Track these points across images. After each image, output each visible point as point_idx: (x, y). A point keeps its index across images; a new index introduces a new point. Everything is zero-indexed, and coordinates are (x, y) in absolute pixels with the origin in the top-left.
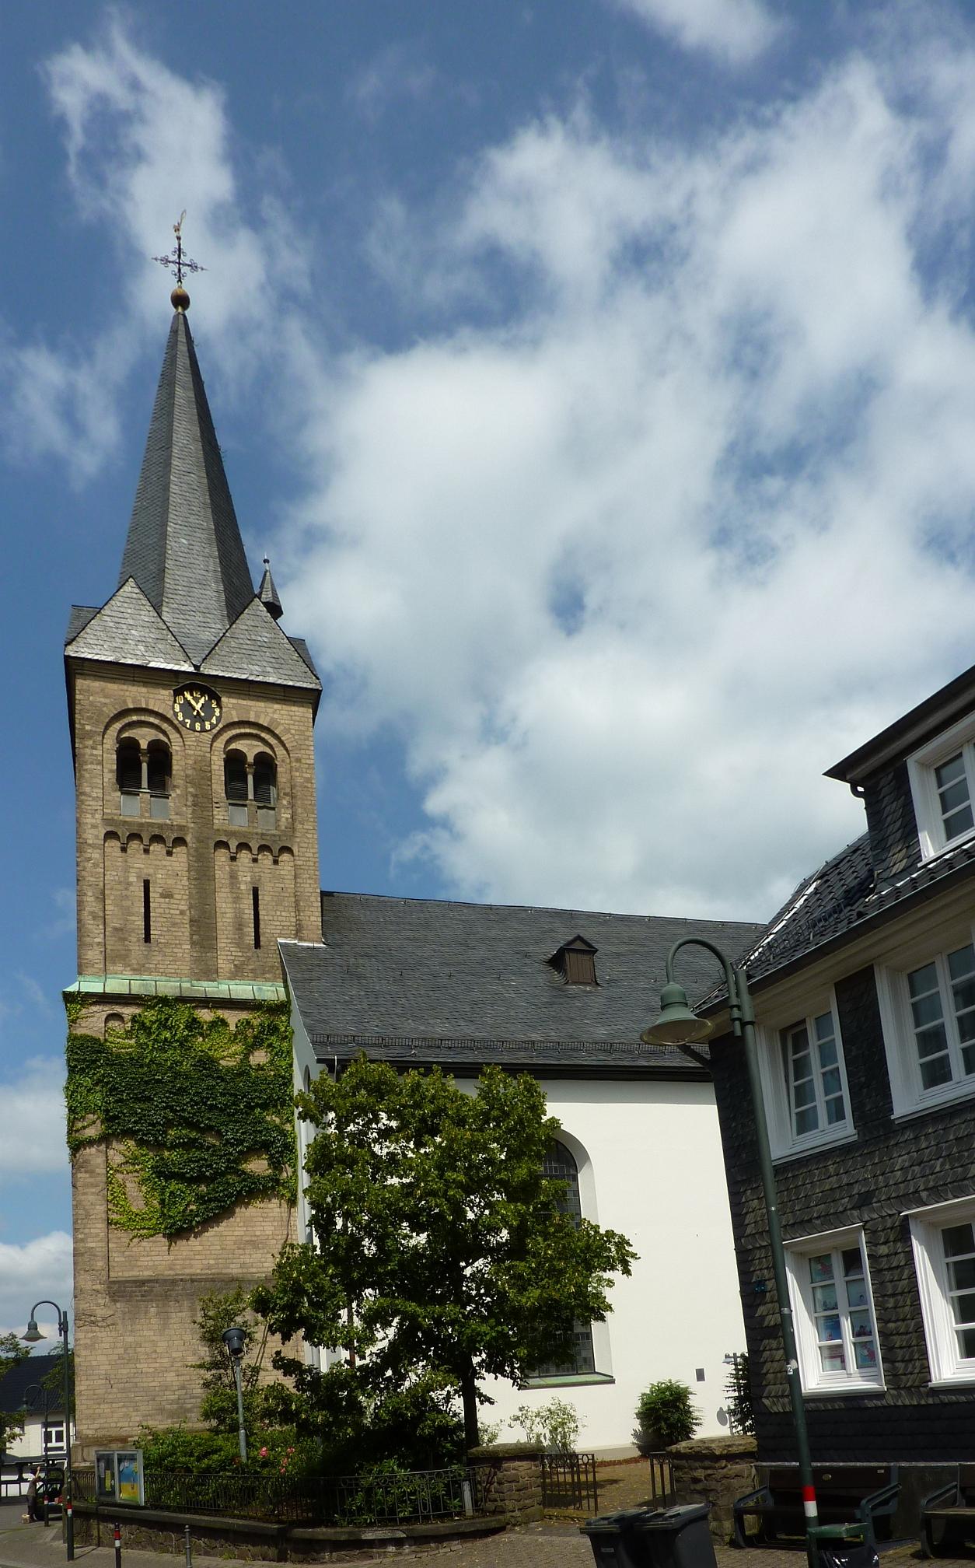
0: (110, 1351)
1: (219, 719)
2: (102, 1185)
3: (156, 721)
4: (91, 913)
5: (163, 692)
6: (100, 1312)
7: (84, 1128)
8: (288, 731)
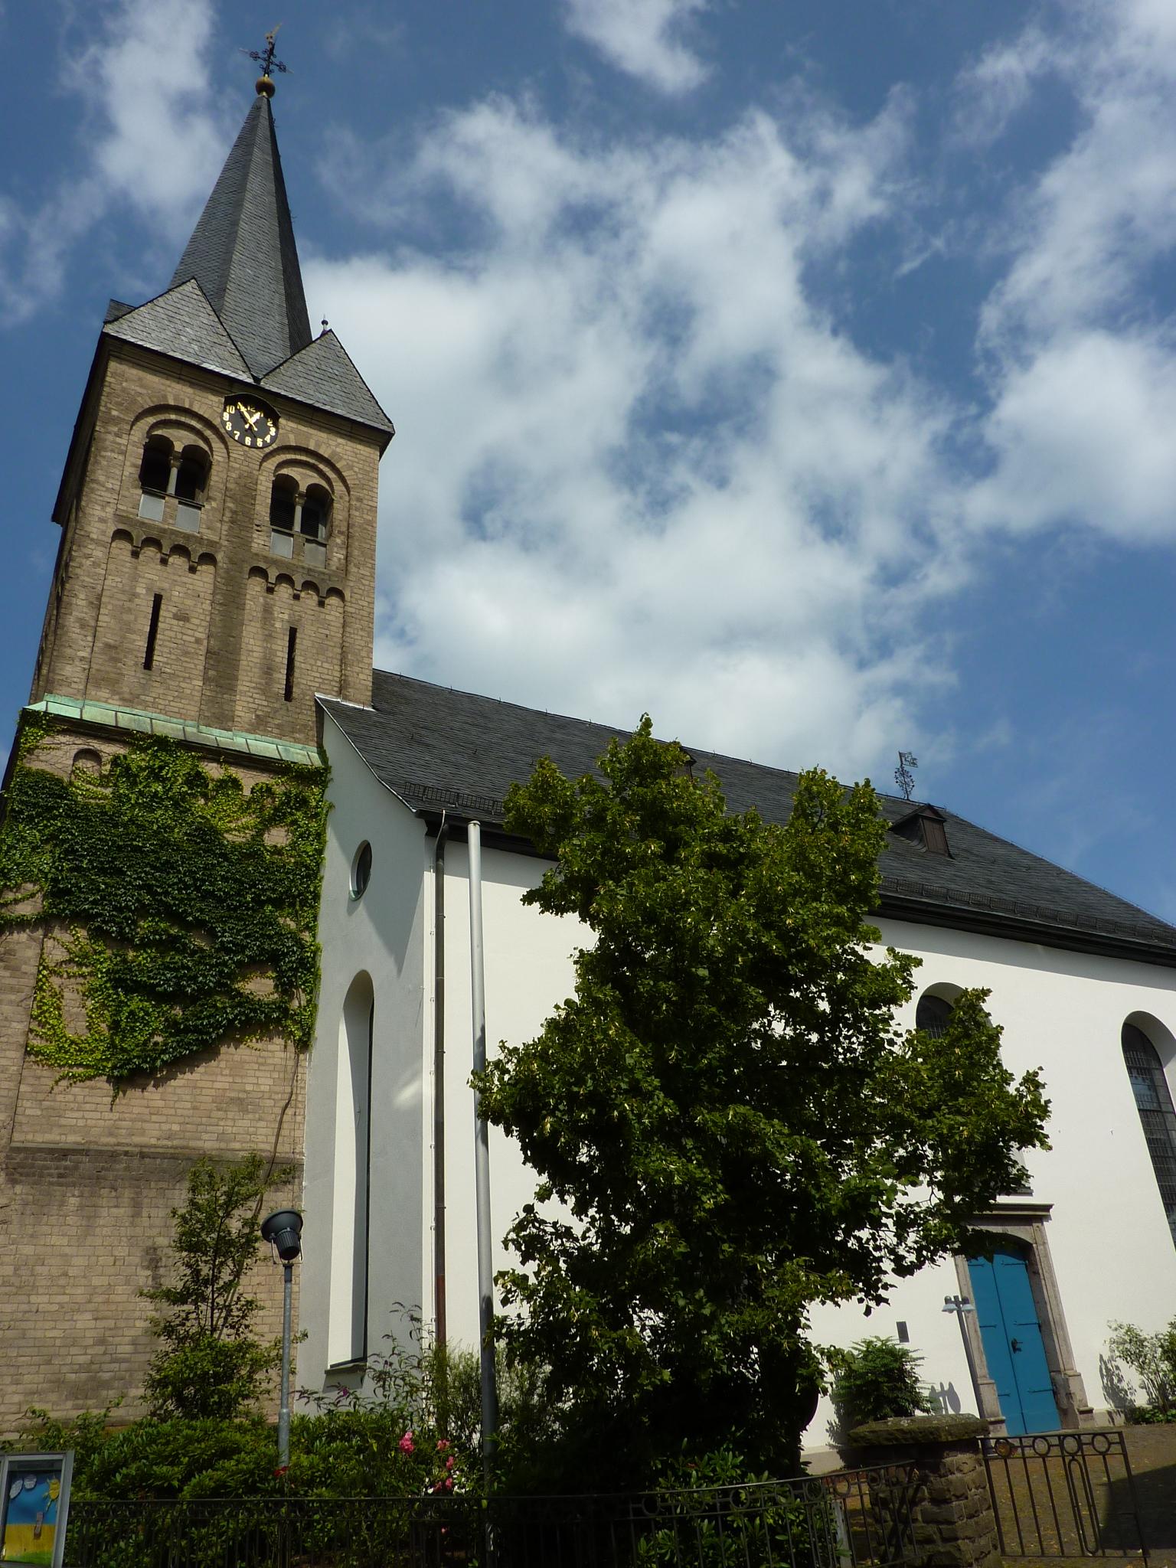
1: (273, 439)
2: (28, 991)
3: (199, 426)
7: (16, 901)
8: (351, 468)
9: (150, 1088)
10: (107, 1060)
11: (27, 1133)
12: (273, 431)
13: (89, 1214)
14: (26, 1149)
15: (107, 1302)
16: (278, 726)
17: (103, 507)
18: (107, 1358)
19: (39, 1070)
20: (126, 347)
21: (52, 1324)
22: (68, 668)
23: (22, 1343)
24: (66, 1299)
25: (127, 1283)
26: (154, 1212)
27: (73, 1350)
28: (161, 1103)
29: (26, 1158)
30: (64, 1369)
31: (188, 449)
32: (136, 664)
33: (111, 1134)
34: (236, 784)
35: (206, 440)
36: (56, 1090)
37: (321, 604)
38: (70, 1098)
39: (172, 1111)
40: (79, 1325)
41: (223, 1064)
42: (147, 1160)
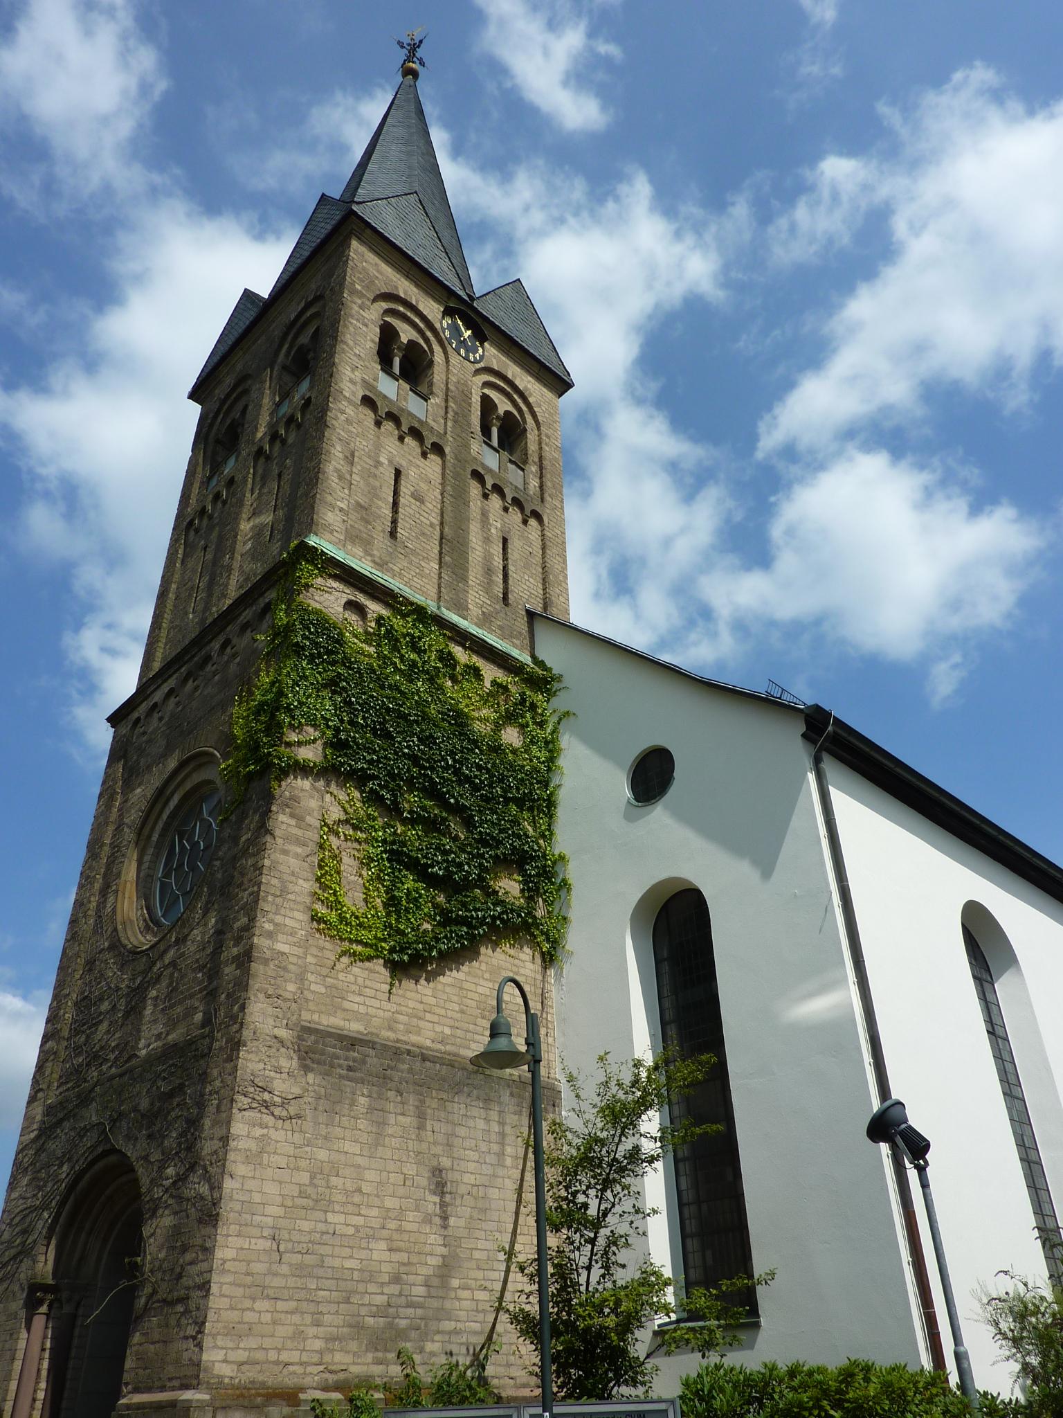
0: (285, 1175)
1: (482, 357)
2: (312, 847)
3: (422, 325)
4: (337, 471)
5: (436, 306)
6: (281, 1086)
7: (300, 744)
8: (540, 406)
9: (423, 981)
10: (384, 940)
11: (313, 1012)
12: (480, 350)
13: (378, 1115)
14: (317, 1031)
15: (399, 1230)
16: (501, 628)
17: (353, 371)
18: (403, 1301)
19: (323, 941)
20: (368, 231)
21: (347, 1251)
22: (330, 514)
23: (321, 1272)
24: (360, 1221)
25: (417, 1209)
26: (437, 1126)
27: (372, 1288)
28: (432, 1001)
29: (317, 1042)
30: (364, 1311)
31: (412, 343)
32: (383, 531)
33: (390, 1028)
34: (476, 673)
35: (427, 340)
36: (338, 967)
37: (525, 522)
38: (351, 978)
39: (443, 1012)
40: (376, 1256)
41: (483, 967)
42: (428, 1064)
